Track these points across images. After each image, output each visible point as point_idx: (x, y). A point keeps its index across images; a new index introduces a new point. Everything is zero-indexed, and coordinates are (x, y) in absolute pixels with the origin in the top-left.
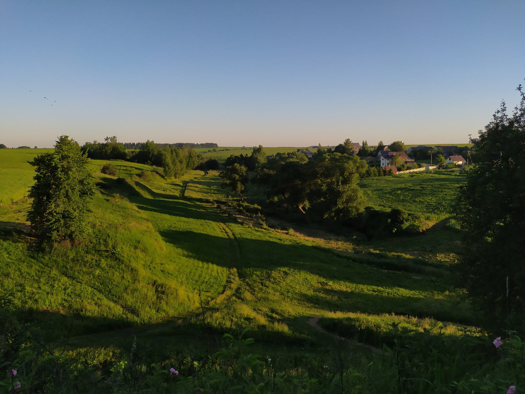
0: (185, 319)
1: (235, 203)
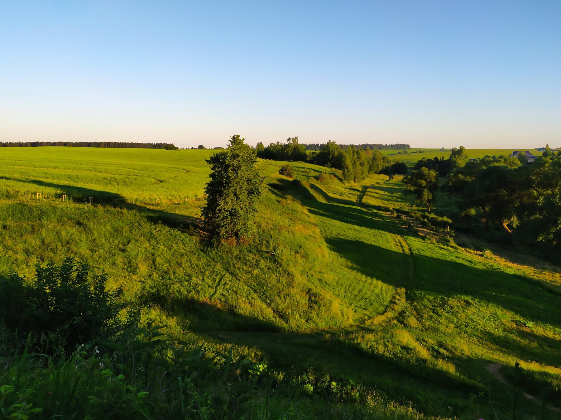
0: (333, 334)
1: (419, 214)
